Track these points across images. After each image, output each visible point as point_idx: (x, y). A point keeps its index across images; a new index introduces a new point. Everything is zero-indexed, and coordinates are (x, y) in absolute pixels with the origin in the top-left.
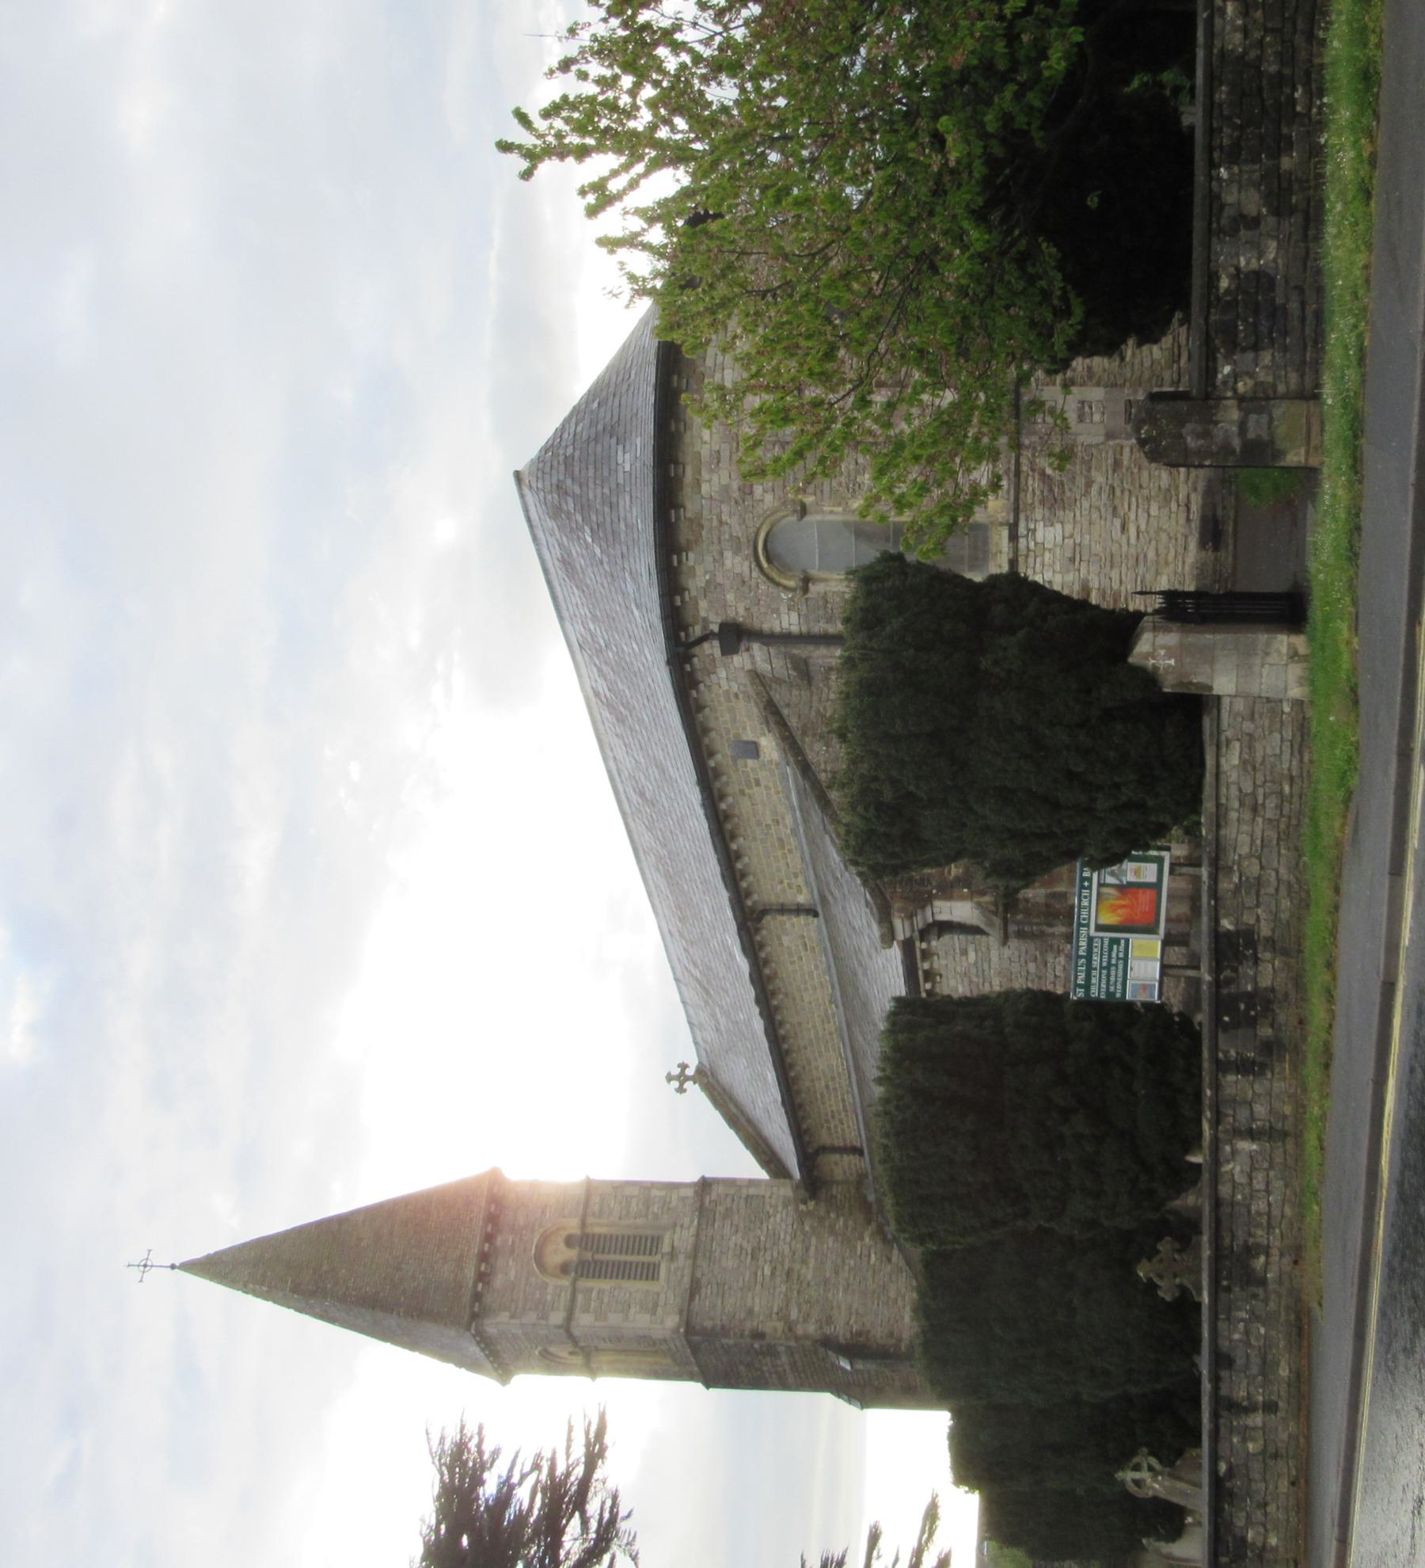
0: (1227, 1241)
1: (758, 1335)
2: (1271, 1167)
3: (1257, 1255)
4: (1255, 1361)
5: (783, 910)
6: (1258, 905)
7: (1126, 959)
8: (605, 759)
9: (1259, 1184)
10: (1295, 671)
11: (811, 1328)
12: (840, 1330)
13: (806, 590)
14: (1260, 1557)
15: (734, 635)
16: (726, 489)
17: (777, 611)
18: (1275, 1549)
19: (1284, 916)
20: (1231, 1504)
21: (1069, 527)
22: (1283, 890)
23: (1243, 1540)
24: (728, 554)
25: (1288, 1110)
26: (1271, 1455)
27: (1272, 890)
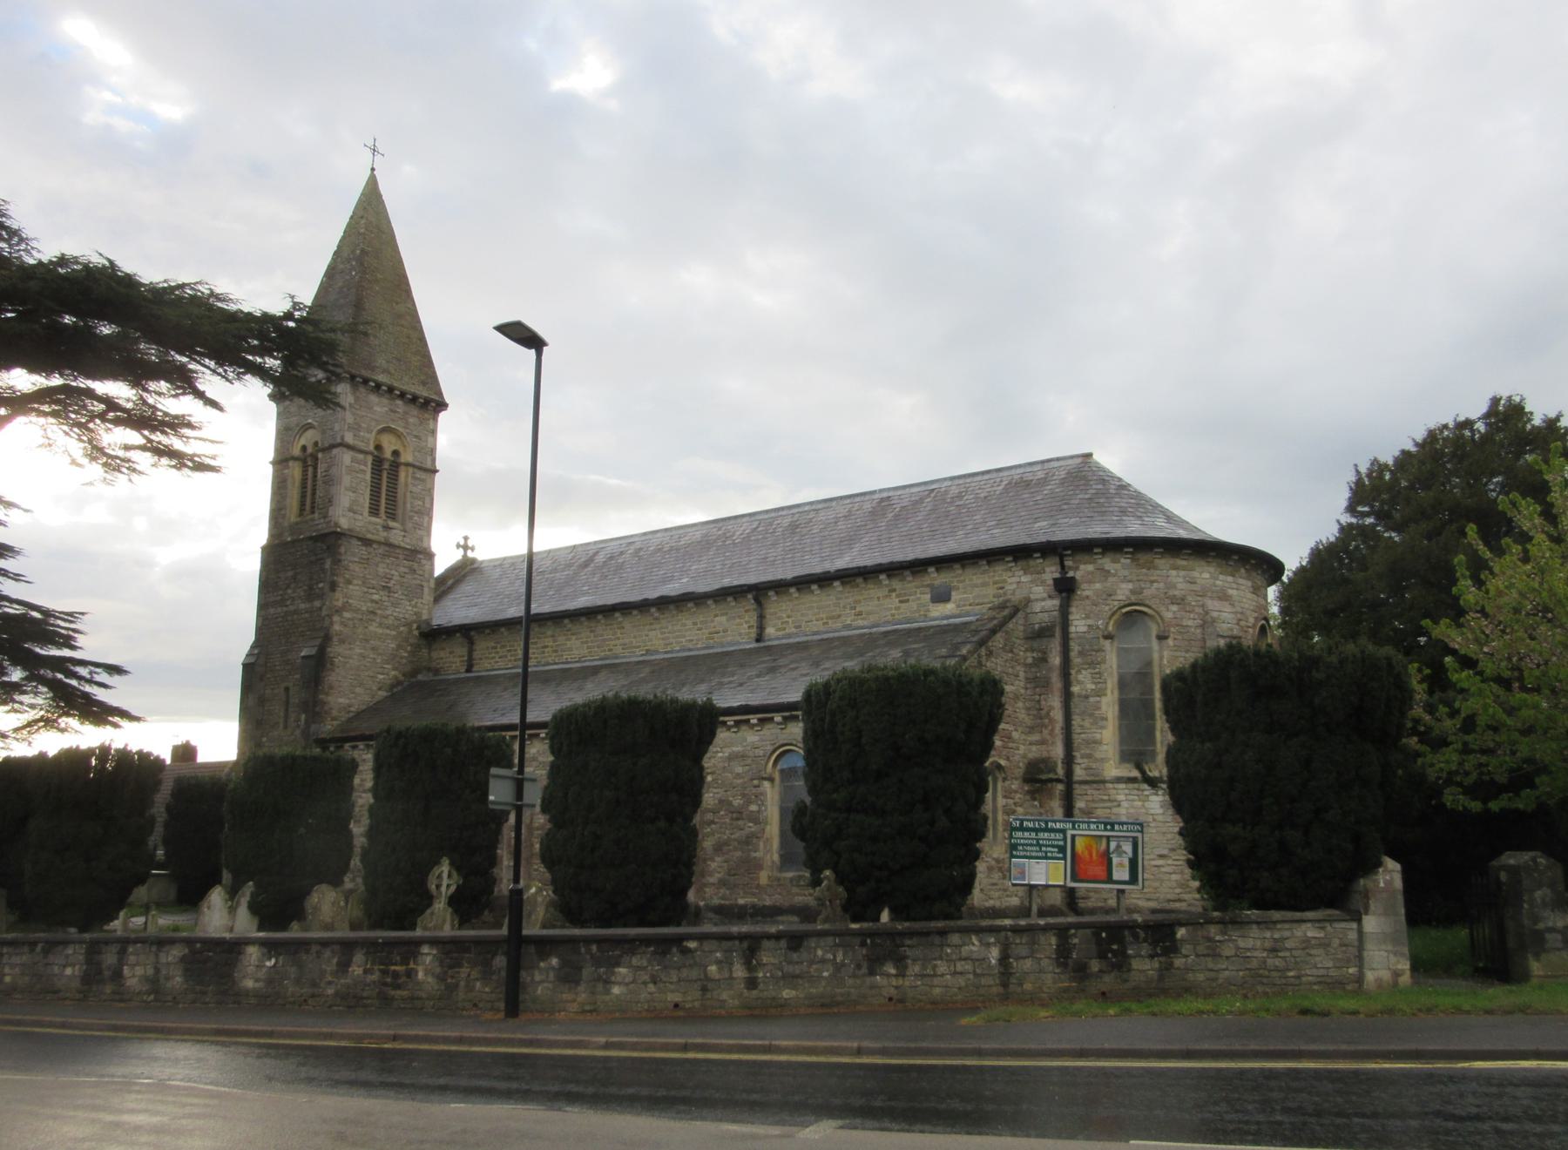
0: (908, 942)
1: (333, 587)
2: (975, 974)
3: (897, 968)
4: (797, 970)
5: (761, 617)
6: (1197, 956)
7: (1046, 858)
8: (811, 503)
9: (960, 967)
10: (1385, 975)
11: (337, 627)
12: (335, 649)
13: (1106, 637)
14: (599, 979)
15: (1065, 588)
16: (1174, 587)
17: (1087, 617)
18: (608, 992)
19: (1190, 976)
20: (655, 953)
21: (1160, 818)
22: (1213, 974)
23: (618, 965)
24: (1130, 586)
25: (1028, 986)
26: (705, 986)
27: (1211, 965)
